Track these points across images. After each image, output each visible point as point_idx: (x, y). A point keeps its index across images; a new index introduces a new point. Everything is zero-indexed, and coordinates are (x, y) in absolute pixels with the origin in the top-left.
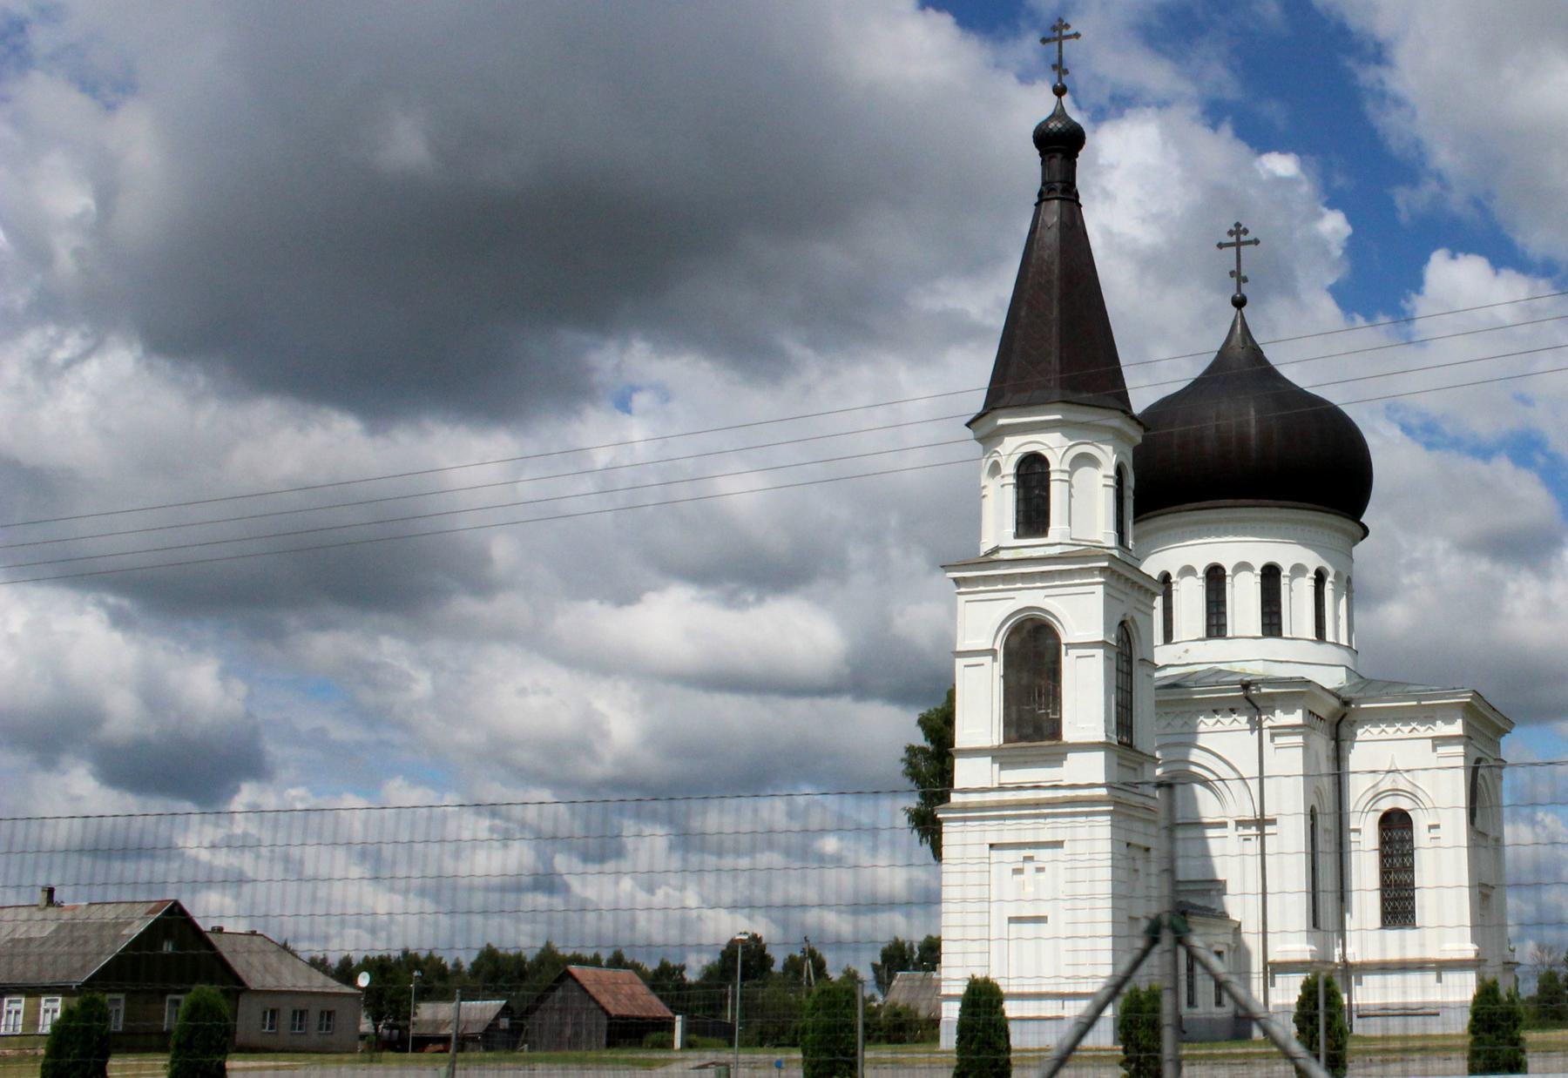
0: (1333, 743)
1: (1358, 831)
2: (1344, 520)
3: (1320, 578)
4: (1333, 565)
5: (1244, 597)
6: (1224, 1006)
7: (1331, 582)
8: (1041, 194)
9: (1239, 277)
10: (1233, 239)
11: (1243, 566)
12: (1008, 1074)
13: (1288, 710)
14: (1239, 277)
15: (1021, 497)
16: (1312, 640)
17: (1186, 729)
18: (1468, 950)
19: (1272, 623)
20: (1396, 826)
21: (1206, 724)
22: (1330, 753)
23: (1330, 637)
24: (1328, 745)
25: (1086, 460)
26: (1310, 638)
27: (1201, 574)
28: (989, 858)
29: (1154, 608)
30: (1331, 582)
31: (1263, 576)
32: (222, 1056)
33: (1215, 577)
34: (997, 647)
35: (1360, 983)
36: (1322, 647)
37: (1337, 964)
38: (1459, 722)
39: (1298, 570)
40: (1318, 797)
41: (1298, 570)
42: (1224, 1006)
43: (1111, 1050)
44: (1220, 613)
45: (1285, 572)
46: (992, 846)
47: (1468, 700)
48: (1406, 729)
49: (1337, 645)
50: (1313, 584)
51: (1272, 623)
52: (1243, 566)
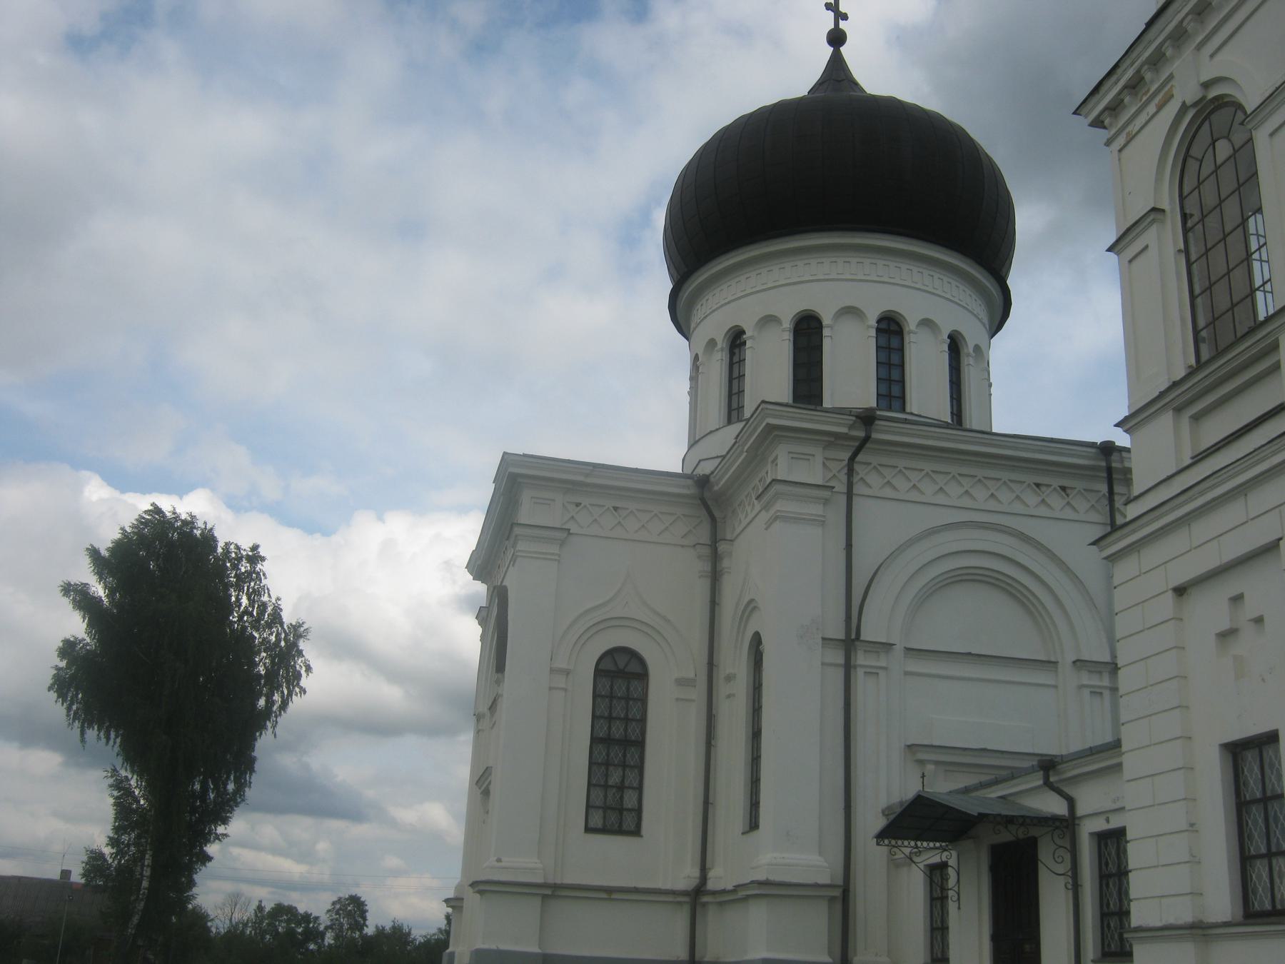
27: (873, 322)
31: (878, 330)
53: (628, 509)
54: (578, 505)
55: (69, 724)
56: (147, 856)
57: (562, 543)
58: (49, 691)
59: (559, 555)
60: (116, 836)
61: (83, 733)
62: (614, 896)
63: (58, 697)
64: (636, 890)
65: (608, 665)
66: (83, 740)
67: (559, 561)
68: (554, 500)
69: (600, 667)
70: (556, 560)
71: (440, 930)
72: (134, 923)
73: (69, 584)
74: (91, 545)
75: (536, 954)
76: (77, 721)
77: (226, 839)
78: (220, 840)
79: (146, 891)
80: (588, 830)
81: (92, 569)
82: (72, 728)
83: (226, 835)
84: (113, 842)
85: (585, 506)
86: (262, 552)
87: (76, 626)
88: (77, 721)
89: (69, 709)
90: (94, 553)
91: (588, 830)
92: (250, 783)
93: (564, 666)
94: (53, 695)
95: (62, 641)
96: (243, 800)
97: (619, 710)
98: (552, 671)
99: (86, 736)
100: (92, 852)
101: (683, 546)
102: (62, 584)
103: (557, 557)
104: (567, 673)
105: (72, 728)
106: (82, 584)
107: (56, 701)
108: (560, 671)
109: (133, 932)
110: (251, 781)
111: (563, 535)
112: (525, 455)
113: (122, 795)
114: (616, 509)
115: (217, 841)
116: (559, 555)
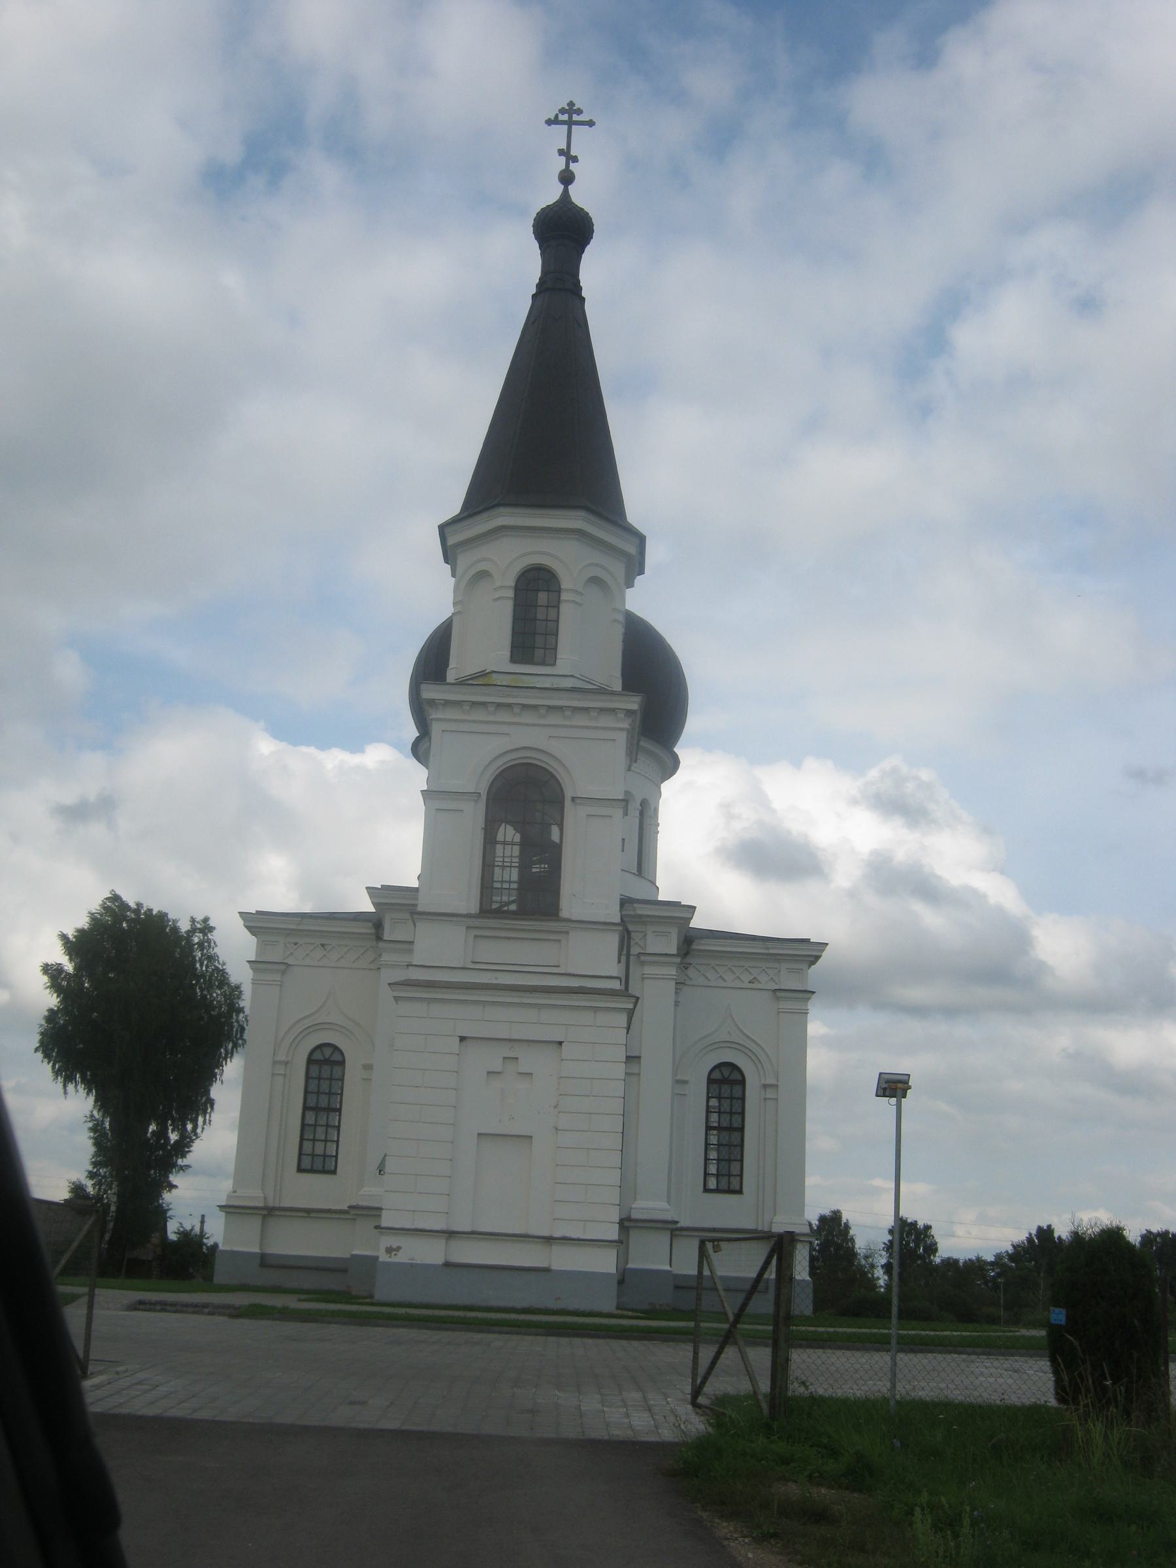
28: (273, 1075)
46: (462, 1039)
48: (746, 978)
53: (331, 945)
54: (296, 944)
55: (54, 1080)
56: (114, 1186)
57: (284, 973)
58: (35, 1052)
59: (280, 981)
60: (95, 1170)
61: (65, 1086)
62: (312, 1215)
63: (45, 1057)
64: (329, 1211)
65: (318, 1056)
66: (65, 1093)
67: (281, 986)
68: (278, 942)
69: (313, 1058)
70: (278, 985)
71: (1007, 1252)
72: (106, 1240)
73: (47, 965)
74: (61, 932)
75: (258, 1253)
76: (59, 1078)
77: (189, 1170)
78: (183, 1170)
79: (114, 1214)
80: (300, 1170)
81: (63, 951)
82: (56, 1082)
83: (188, 1166)
84: (91, 1175)
85: (301, 945)
86: (212, 923)
87: (52, 1000)
88: (59, 1078)
89: (53, 1067)
90: (64, 937)
91: (300, 1170)
92: (210, 1121)
93: (284, 1058)
94: (40, 1055)
95: (48, 1010)
96: (197, 1137)
97: (325, 1086)
98: (275, 1063)
99: (67, 1088)
100: (73, 1183)
101: (370, 969)
102: (42, 964)
103: (279, 983)
104: (286, 1063)
105: (56, 1082)
106: (57, 964)
107: (42, 1062)
108: (280, 1062)
109: (106, 1246)
110: (212, 1119)
111: (283, 967)
112: (259, 913)
113: (99, 1136)
114: (323, 945)
115: (181, 1171)
116: (280, 981)
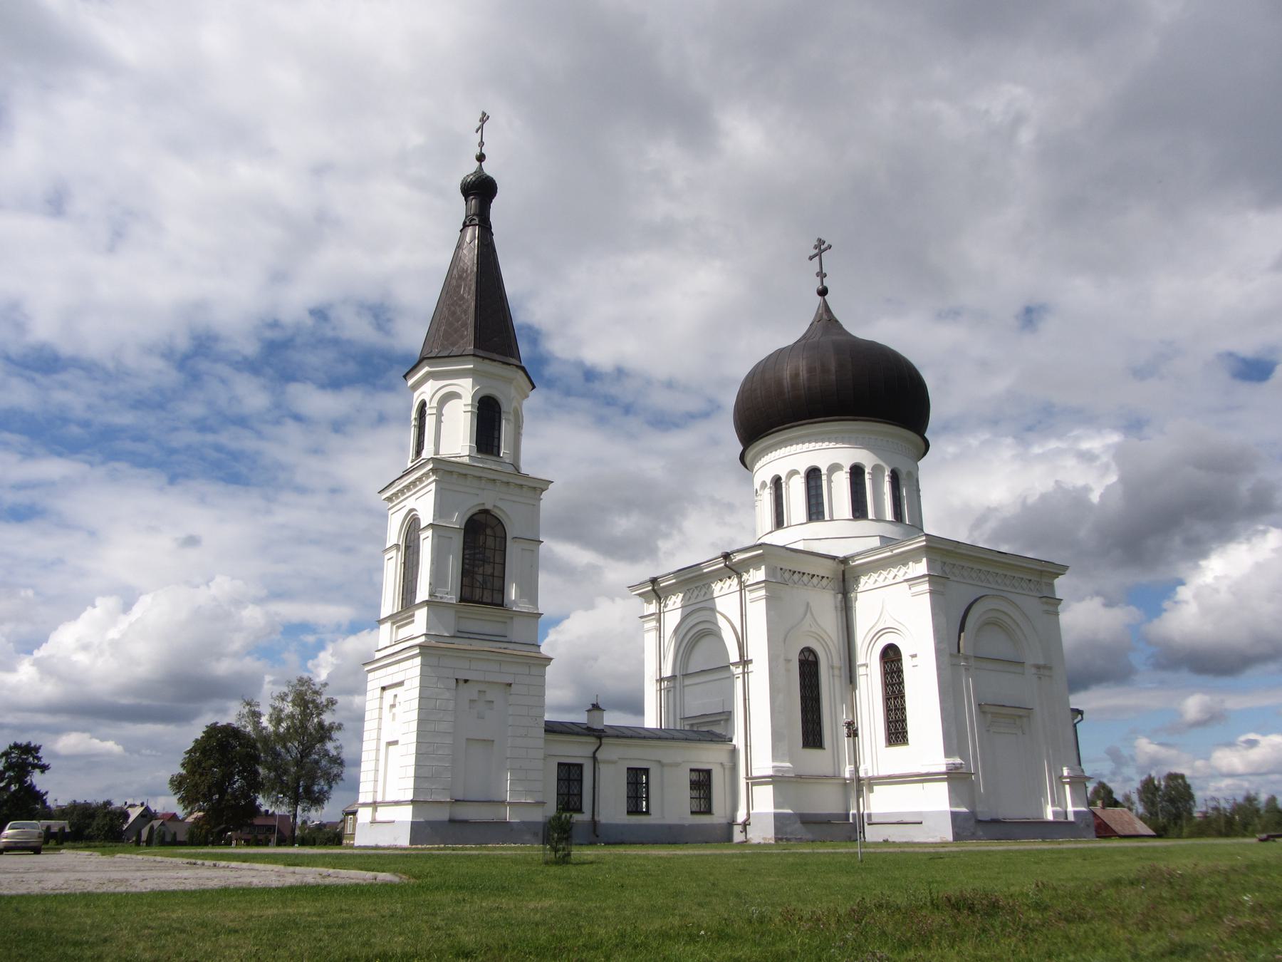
0: (840, 596)
1: (866, 665)
2: (882, 425)
3: (857, 473)
4: (888, 464)
5: (796, 494)
6: (583, 813)
7: (869, 473)
8: (465, 223)
9: (821, 275)
10: (817, 251)
11: (794, 473)
12: (1279, 811)
13: (758, 568)
14: (821, 275)
15: (496, 440)
16: (892, 521)
17: (707, 597)
18: (938, 761)
19: (815, 510)
20: (891, 657)
21: (717, 588)
22: (839, 605)
23: (871, 515)
24: (835, 597)
25: (453, 396)
26: (890, 519)
27: (803, 474)
29: (541, 499)
30: (869, 473)
32: (91, 820)
33: (777, 481)
34: (400, 543)
35: (871, 791)
36: (861, 524)
37: (845, 779)
38: (924, 560)
39: (834, 468)
40: (703, 636)
41: (834, 468)
42: (583, 813)
43: (405, 849)
44: (819, 512)
45: (824, 471)
46: (384, 689)
47: (924, 543)
49: (879, 519)
50: (849, 476)
51: (815, 510)
52: (794, 473)
